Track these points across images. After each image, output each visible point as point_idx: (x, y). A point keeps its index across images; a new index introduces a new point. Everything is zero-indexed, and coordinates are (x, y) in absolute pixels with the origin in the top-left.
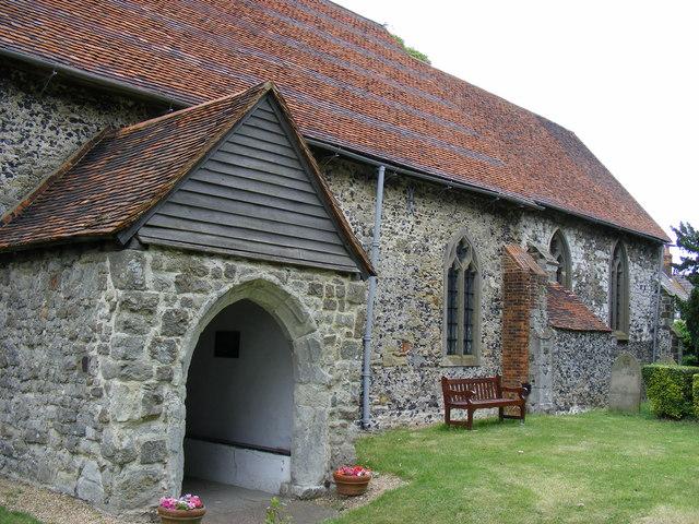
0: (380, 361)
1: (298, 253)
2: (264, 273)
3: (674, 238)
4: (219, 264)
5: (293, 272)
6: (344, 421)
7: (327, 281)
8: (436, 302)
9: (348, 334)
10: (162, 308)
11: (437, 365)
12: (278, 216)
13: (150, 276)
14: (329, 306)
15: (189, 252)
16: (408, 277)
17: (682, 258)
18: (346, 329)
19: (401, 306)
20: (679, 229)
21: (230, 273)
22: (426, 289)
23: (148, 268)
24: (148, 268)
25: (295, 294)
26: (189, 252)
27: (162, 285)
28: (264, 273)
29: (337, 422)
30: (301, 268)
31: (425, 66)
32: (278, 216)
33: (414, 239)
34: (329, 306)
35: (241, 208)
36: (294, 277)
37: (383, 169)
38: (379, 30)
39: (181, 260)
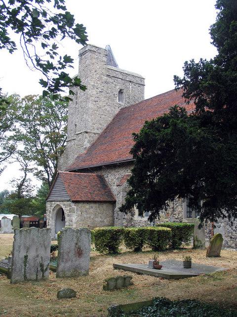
2: (58, 203)
4: (53, 203)
7: (65, 203)
12: (61, 193)
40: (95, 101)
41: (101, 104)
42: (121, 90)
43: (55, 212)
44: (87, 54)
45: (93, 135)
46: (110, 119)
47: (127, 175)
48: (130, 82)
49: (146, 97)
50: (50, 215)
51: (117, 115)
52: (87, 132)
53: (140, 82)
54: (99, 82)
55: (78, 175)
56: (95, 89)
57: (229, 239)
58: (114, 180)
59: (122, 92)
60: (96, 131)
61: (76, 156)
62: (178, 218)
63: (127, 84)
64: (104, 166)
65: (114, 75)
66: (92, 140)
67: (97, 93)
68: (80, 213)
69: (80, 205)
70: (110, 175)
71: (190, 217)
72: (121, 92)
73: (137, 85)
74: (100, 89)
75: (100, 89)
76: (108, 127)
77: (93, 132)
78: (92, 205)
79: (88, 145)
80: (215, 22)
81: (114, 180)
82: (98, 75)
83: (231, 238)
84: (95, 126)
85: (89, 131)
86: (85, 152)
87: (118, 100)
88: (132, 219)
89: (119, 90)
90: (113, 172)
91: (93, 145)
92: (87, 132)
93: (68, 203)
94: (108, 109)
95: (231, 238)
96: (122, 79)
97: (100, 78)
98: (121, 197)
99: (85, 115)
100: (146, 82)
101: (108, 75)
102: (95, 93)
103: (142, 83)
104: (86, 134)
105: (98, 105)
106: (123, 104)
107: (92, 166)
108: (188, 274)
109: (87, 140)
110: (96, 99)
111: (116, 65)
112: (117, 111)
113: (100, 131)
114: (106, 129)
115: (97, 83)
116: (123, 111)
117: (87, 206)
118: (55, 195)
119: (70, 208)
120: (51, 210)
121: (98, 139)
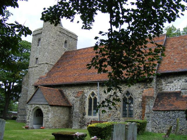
0: (103, 118)
1: (42, 103)
2: (38, 106)
3: (32, 35)
4: (34, 105)
7: (44, 106)
8: (119, 106)
11: (119, 120)
12: (40, 99)
13: (29, 107)
14: (44, 109)
15: (31, 104)
20: (16, 7)
26: (31, 104)
28: (38, 106)
30: (41, 105)
31: (56, 10)
32: (40, 99)
34: (44, 109)
35: (36, 99)
38: (18, 4)
39: (31, 105)
41: (55, 47)
42: (66, 41)
43: (34, 111)
45: (50, 65)
46: (60, 57)
47: (81, 91)
49: (77, 49)
51: (63, 55)
52: (47, 63)
53: (75, 38)
55: (47, 88)
57: (155, 129)
58: (71, 94)
60: (52, 63)
62: (117, 117)
63: (69, 38)
64: (64, 85)
65: (63, 32)
66: (49, 68)
68: (53, 112)
69: (53, 108)
70: (67, 90)
71: (125, 117)
72: (66, 42)
74: (55, 39)
75: (55, 39)
76: (58, 62)
77: (50, 63)
78: (59, 108)
79: (47, 71)
80: (134, 9)
81: (71, 94)
83: (156, 128)
84: (52, 60)
85: (48, 63)
86: (46, 75)
88: (83, 117)
90: (70, 89)
91: (50, 71)
92: (47, 63)
93: (47, 106)
94: (59, 51)
95: (156, 128)
96: (67, 35)
97: (56, 33)
98: (78, 104)
99: (46, 53)
100: (78, 39)
101: (60, 31)
102: (53, 41)
103: (76, 39)
106: (67, 50)
107: (55, 84)
110: (53, 44)
111: (62, 27)
113: (54, 64)
117: (57, 108)
118: (35, 101)
119: (48, 110)
120: (32, 110)
121: (53, 68)
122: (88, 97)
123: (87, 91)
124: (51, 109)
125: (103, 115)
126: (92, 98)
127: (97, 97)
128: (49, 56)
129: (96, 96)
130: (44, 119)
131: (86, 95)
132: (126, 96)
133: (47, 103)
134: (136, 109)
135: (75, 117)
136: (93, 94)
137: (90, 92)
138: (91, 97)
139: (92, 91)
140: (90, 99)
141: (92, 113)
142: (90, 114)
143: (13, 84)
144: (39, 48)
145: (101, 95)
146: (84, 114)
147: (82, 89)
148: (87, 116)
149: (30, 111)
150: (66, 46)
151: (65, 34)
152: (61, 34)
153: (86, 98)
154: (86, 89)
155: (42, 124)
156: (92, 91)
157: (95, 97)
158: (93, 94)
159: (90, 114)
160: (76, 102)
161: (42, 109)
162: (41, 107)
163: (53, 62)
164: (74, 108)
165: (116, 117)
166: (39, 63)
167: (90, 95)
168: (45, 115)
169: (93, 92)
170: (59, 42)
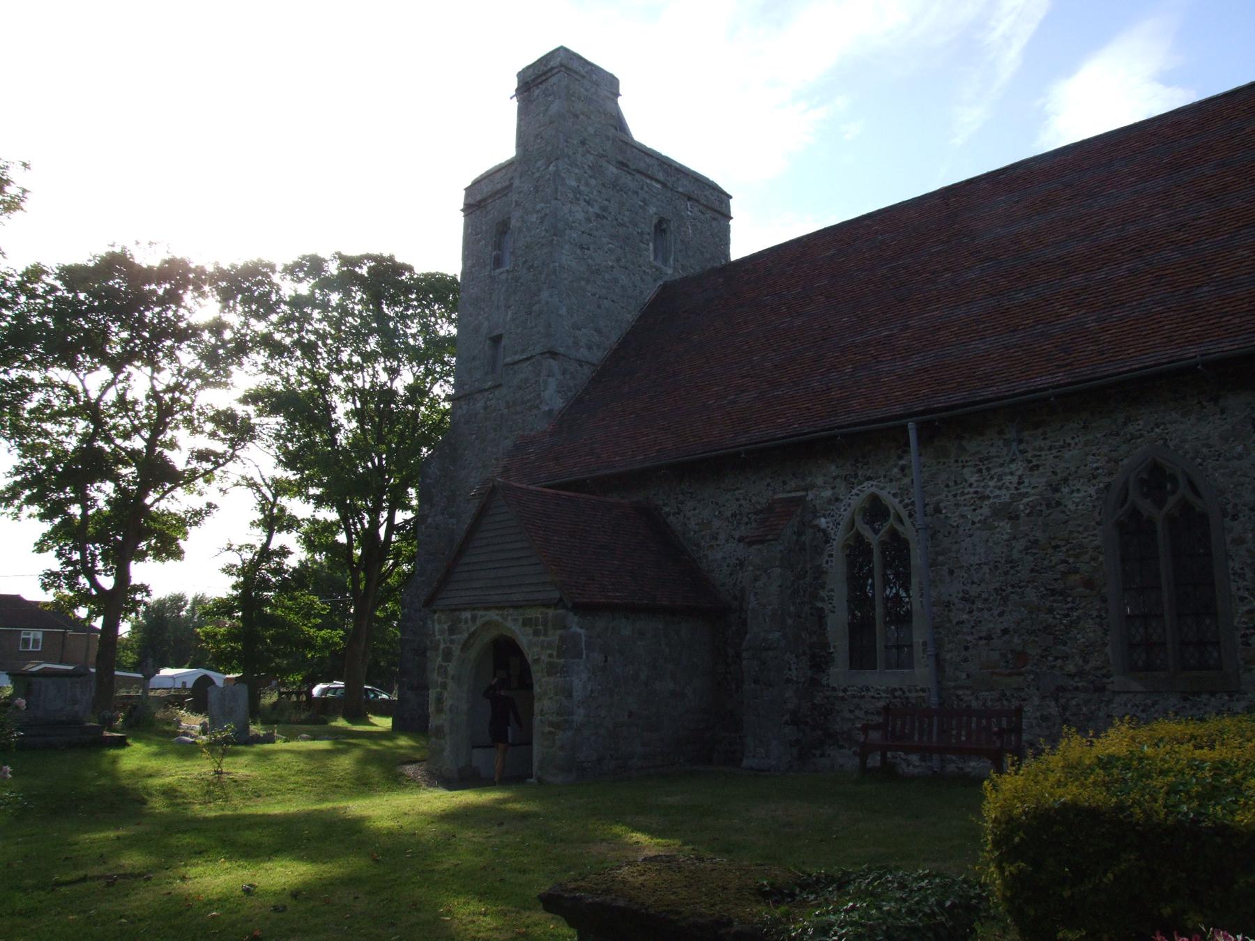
2: (493, 615)
4: (467, 615)
5: (511, 611)
6: (552, 730)
8: (1088, 584)
9: (551, 656)
10: (442, 646)
11: (1101, 689)
14: (536, 633)
16: (1015, 555)
17: (228, 570)
18: (549, 651)
19: (1005, 600)
21: (474, 618)
22: (1062, 567)
23: (436, 623)
24: (436, 623)
25: (513, 628)
27: (442, 633)
29: (547, 729)
30: (516, 607)
33: (1026, 495)
34: (536, 633)
36: (511, 615)
37: (911, 426)
40: (582, 247)
42: (661, 221)
44: (553, 80)
46: (630, 317)
48: (689, 199)
50: (452, 668)
54: (593, 182)
56: (583, 203)
58: (716, 523)
59: (664, 231)
60: (583, 353)
61: (508, 443)
67: (588, 220)
72: (661, 228)
73: (709, 214)
76: (625, 342)
79: (559, 403)
81: (716, 523)
82: (591, 158)
85: (561, 350)
87: (652, 258)
89: (655, 221)
92: (553, 354)
99: (545, 295)
102: (580, 216)
104: (553, 362)
105: (590, 261)
108: (299, 726)
109: (553, 384)
112: (650, 291)
113: (597, 356)
114: (200, 853)
115: (587, 184)
116: (669, 295)
122: (839, 537)
123: (828, 493)
124: (582, 631)
125: (966, 660)
126: (873, 539)
127: (908, 531)
128: (563, 311)
129: (900, 528)
130: (537, 706)
131: (823, 522)
132: (1147, 507)
133: (556, 595)
134: (1242, 599)
135: (756, 682)
136: (876, 511)
137: (855, 500)
138: (859, 537)
139: (869, 488)
140: (858, 551)
141: (880, 645)
142: (861, 657)
143: (391, 519)
144: (504, 277)
145: (938, 510)
146: (820, 661)
147: (793, 484)
148: (839, 674)
149: (447, 656)
150: (662, 253)
151: (652, 178)
152: (626, 179)
153: (827, 542)
154: (819, 481)
155: (529, 743)
156: (868, 491)
157: (894, 534)
158: (876, 511)
159: (861, 657)
160: (756, 579)
161: (524, 638)
162: (513, 626)
163: (589, 348)
164: (146, 666)
165: (1071, 668)
166: (508, 360)
167: (852, 524)
168: (542, 682)
169: (875, 500)
170: (621, 225)
